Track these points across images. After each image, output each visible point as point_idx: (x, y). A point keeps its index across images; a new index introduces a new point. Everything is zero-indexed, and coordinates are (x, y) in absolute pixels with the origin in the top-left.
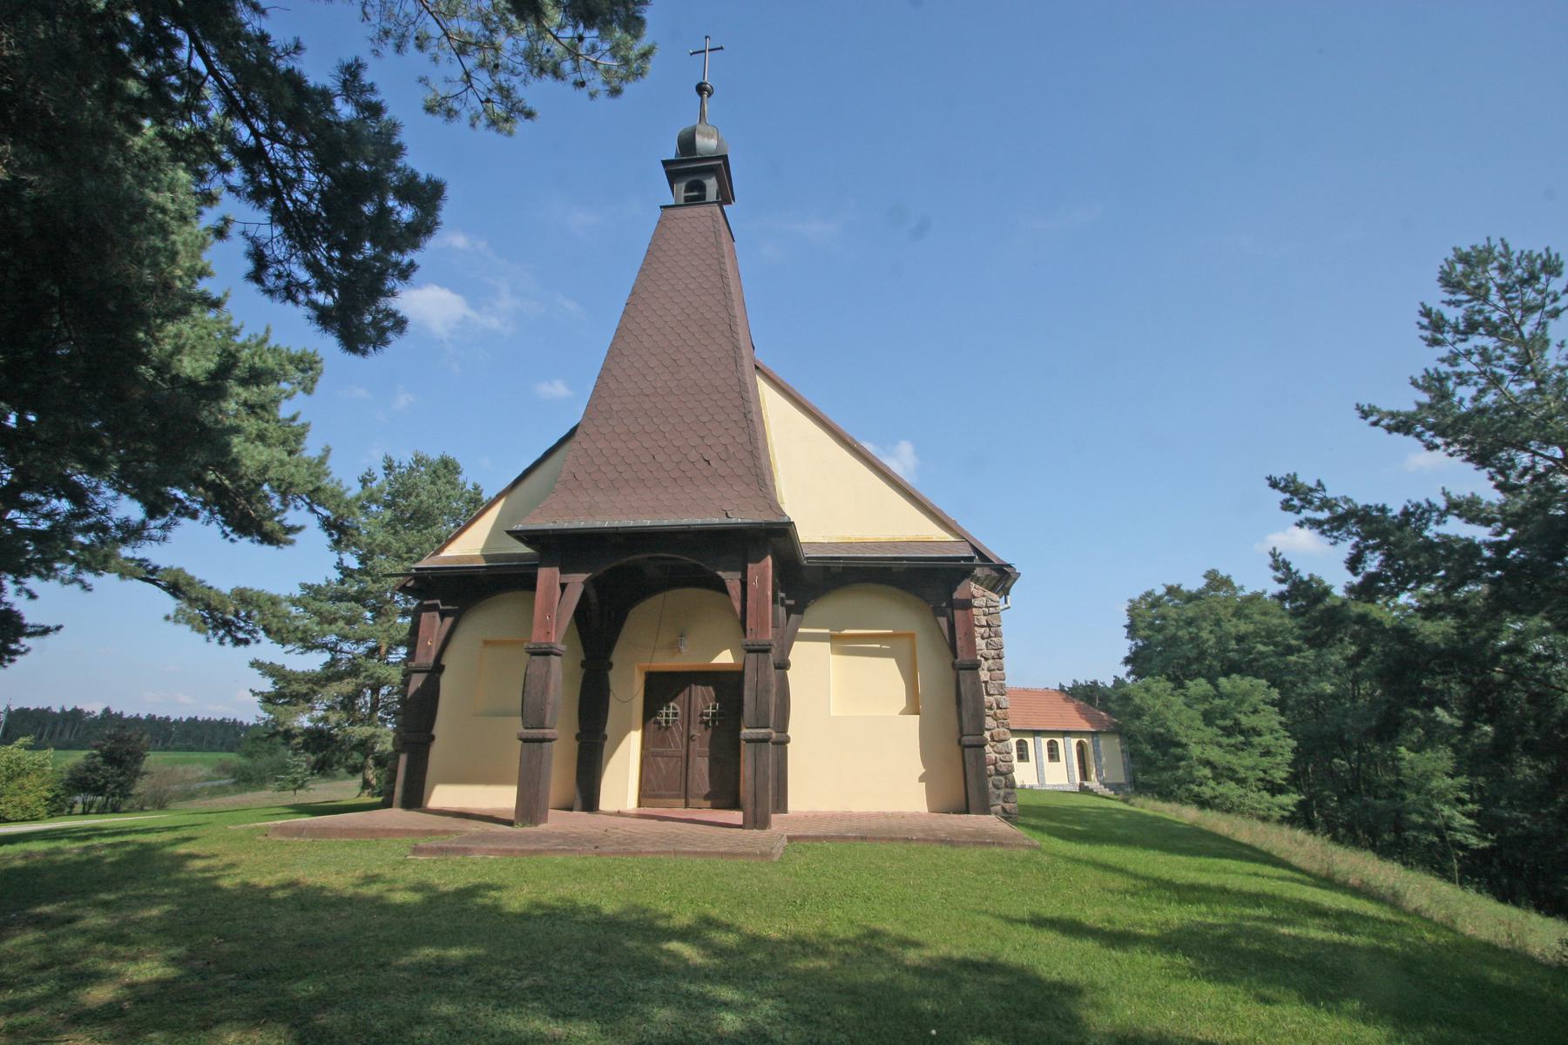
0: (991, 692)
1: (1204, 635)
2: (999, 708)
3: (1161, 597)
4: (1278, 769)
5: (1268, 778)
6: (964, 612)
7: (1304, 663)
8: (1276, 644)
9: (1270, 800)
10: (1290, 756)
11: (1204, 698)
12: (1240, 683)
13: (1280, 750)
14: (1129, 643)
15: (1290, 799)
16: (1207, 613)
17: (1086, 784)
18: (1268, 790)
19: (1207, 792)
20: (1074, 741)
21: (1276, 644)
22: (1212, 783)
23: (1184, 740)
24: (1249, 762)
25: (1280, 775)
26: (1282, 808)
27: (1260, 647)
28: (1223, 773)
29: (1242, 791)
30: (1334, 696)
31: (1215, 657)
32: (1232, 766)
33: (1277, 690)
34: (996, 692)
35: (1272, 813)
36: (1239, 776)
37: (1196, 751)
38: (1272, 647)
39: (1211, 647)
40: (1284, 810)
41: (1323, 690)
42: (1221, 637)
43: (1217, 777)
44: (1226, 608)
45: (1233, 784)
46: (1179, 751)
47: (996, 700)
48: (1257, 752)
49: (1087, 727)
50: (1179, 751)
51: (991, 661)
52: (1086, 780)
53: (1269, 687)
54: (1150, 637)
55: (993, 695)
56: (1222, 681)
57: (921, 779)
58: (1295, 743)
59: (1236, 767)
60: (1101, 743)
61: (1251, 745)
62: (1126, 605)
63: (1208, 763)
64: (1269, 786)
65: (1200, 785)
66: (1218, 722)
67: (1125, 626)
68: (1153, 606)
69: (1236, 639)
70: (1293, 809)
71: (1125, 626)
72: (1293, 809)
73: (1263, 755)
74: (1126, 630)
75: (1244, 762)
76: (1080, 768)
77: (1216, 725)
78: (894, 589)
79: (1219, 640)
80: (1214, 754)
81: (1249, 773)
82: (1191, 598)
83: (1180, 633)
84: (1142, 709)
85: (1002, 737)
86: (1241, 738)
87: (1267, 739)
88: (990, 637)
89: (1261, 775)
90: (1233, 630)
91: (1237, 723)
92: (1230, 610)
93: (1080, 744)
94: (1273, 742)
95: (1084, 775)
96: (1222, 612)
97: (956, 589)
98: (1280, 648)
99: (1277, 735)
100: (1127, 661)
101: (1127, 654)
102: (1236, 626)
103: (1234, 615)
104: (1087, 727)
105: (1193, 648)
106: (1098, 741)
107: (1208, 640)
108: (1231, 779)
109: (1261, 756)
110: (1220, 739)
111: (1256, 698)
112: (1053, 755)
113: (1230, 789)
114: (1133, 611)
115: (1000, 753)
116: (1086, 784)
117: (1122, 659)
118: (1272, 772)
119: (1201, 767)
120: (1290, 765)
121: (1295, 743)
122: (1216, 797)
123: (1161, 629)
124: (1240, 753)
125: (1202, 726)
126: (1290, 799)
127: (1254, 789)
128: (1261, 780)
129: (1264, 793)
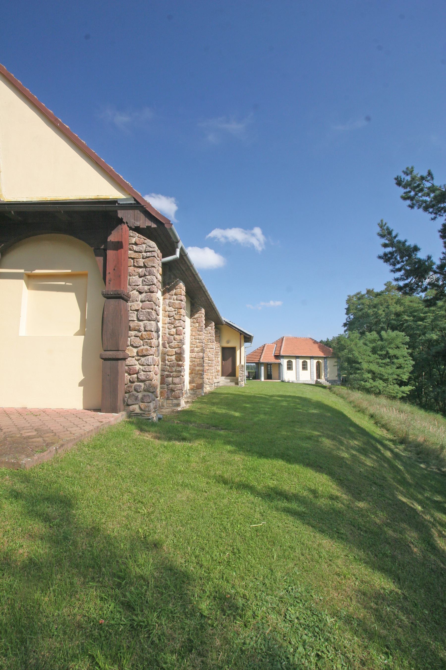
0: (141, 318)
1: (380, 312)
2: (145, 331)
3: (363, 296)
4: (405, 375)
5: (400, 379)
6: (115, 252)
7: (425, 325)
8: (414, 316)
9: (399, 388)
10: (411, 369)
11: (374, 341)
12: (389, 334)
13: (406, 366)
14: (346, 316)
15: (407, 389)
16: (383, 302)
17: (319, 380)
18: (398, 384)
19: (368, 385)
20: (315, 361)
21: (414, 316)
22: (371, 381)
23: (360, 361)
24: (390, 371)
25: (405, 377)
26: (403, 392)
27: (406, 318)
28: (375, 376)
29: (385, 385)
30: (437, 341)
31: (384, 323)
32: (382, 373)
33: (408, 337)
34: (145, 319)
35: (398, 395)
36: (385, 378)
37: (365, 366)
38: (412, 318)
39: (383, 318)
40: (404, 393)
41: (432, 338)
42: (387, 313)
43: (374, 379)
44: (392, 299)
45: (381, 382)
46: (358, 365)
47: (144, 324)
48: (395, 367)
49: (322, 355)
50: (358, 365)
51: (144, 294)
52: (320, 378)
53: (405, 336)
54: (356, 313)
55: (142, 321)
56: (383, 333)
57: (81, 384)
58: (414, 363)
59: (384, 374)
60: (328, 362)
61: (393, 363)
62: (346, 298)
63: (370, 371)
64: (399, 382)
65: (366, 381)
66: (379, 352)
67: (346, 309)
68: (359, 299)
69: (395, 314)
70: (409, 393)
71: (346, 309)
72: (409, 393)
73: (398, 368)
74: (346, 310)
75: (387, 371)
76: (317, 373)
77: (378, 354)
78: (83, 242)
79: (387, 315)
80: (374, 367)
81: (389, 376)
82: (378, 295)
83: (369, 311)
84: (345, 346)
85: (145, 353)
86: (388, 360)
87: (401, 361)
88: (145, 275)
89: (396, 377)
90: (393, 310)
91: (388, 353)
92: (394, 301)
93: (318, 363)
94: (403, 362)
95: (319, 376)
96: (390, 301)
97: (111, 233)
98: (415, 318)
99: (405, 359)
100: (345, 325)
101: (345, 321)
102: (395, 308)
103: (396, 303)
104: (322, 355)
105: (374, 318)
106: (326, 361)
107: (381, 314)
108: (381, 379)
109: (396, 369)
110: (378, 360)
111: (398, 342)
112: (305, 367)
113: (380, 384)
114: (349, 301)
115: (143, 365)
116: (319, 380)
117: (342, 324)
118: (401, 375)
119: (367, 373)
120: (410, 373)
121: (414, 363)
122: (372, 387)
123: (361, 310)
124: (387, 367)
125: (370, 354)
126: (407, 389)
127: (392, 383)
128: (396, 379)
129: (396, 385)
